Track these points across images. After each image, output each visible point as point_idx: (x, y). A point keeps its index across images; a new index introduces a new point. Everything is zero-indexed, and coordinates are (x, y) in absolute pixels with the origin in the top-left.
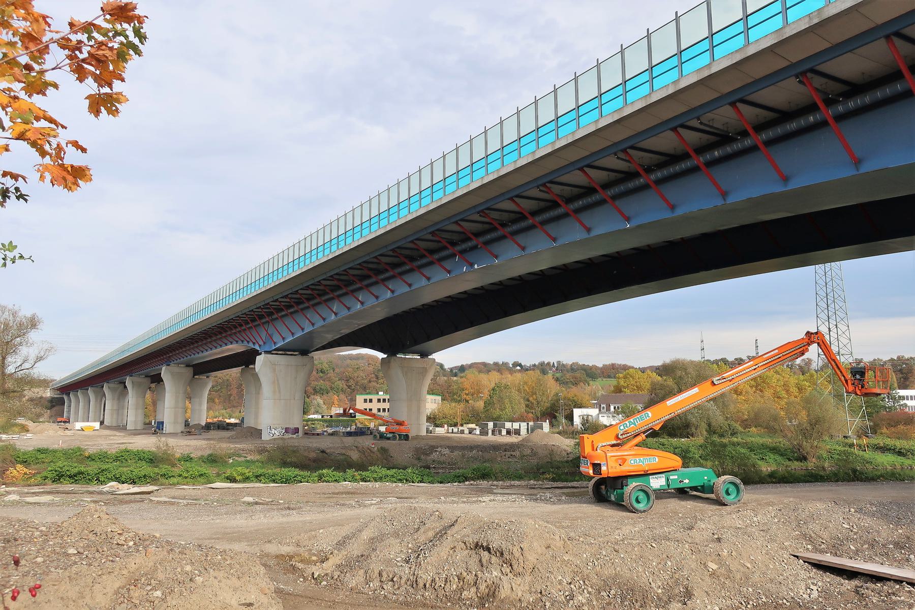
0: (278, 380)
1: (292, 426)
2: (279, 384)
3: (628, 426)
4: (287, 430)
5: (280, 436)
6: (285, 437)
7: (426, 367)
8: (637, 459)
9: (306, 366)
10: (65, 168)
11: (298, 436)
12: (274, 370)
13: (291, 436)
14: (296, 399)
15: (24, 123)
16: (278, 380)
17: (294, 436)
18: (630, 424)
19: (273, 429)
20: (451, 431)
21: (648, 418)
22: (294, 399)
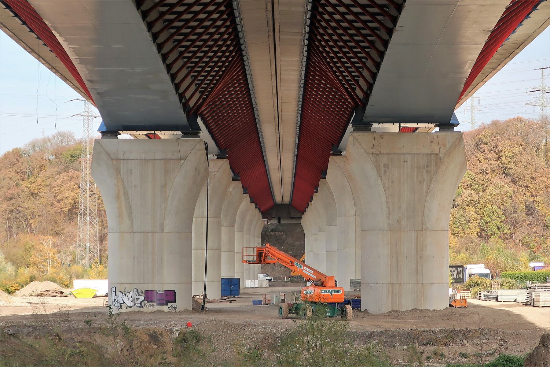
0: (126, 193)
1: (159, 287)
2: (127, 200)
3: (327, 292)
4: (149, 296)
5: (135, 309)
6: (145, 309)
7: (437, 151)
8: (327, 290)
9: (185, 158)
10: (279, 232)
11: (175, 308)
12: (118, 171)
13: (157, 307)
14: (167, 229)
15: (186, 159)
16: (126, 193)
17: (165, 308)
18: (328, 291)
19: (120, 294)
20: (123, 302)
21: (339, 293)
22: (162, 231)
